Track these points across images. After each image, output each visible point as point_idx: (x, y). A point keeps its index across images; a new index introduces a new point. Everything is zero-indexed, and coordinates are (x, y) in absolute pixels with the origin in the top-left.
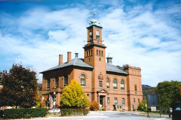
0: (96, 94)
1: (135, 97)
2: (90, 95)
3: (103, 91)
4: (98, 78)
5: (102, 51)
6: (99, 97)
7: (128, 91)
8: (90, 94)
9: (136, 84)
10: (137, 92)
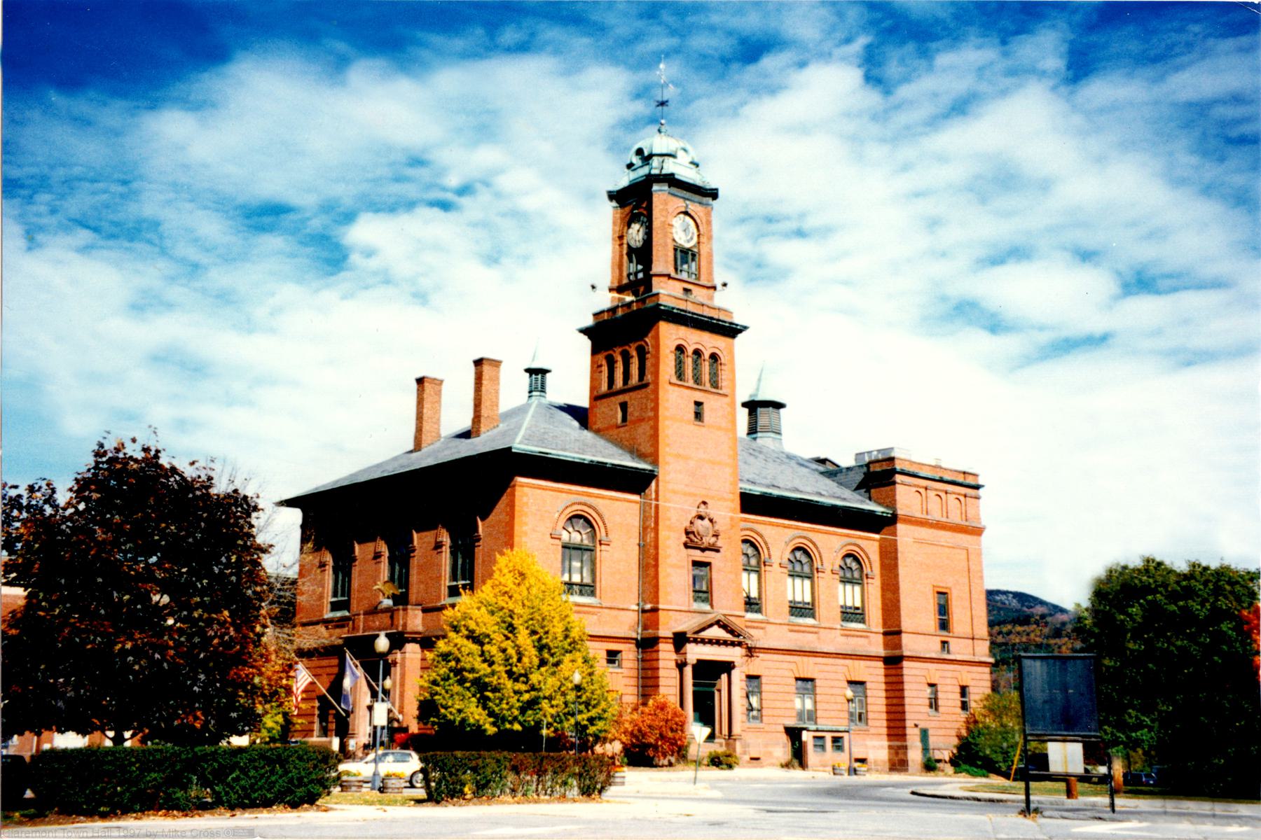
0: (666, 653)
1: (935, 672)
2: (624, 655)
3: (716, 632)
4: (684, 538)
5: (714, 357)
6: (688, 671)
7: (893, 633)
8: (629, 654)
9: (946, 582)
10: (954, 644)
